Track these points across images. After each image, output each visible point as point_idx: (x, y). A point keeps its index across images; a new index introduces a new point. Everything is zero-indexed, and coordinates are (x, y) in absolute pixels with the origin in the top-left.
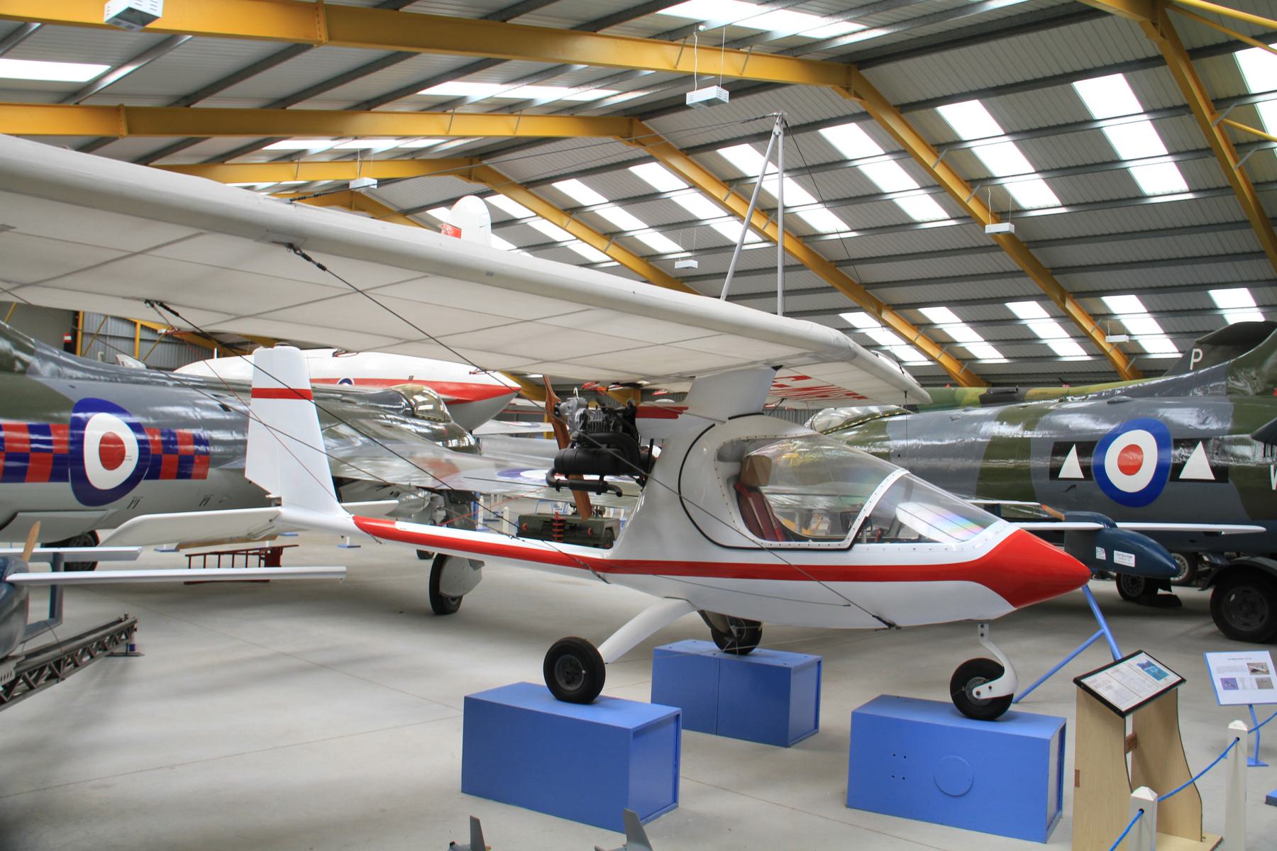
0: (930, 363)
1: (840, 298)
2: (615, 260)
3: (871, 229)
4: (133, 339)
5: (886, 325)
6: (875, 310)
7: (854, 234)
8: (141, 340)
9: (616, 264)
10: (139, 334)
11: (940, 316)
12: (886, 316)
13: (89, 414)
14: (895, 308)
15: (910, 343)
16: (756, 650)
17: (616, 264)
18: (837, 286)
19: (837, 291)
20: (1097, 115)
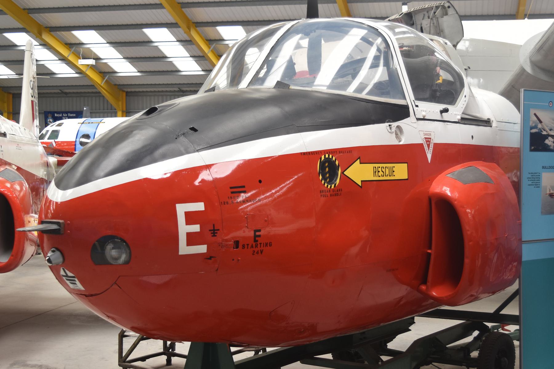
5: (45, 45)
15: (63, 59)
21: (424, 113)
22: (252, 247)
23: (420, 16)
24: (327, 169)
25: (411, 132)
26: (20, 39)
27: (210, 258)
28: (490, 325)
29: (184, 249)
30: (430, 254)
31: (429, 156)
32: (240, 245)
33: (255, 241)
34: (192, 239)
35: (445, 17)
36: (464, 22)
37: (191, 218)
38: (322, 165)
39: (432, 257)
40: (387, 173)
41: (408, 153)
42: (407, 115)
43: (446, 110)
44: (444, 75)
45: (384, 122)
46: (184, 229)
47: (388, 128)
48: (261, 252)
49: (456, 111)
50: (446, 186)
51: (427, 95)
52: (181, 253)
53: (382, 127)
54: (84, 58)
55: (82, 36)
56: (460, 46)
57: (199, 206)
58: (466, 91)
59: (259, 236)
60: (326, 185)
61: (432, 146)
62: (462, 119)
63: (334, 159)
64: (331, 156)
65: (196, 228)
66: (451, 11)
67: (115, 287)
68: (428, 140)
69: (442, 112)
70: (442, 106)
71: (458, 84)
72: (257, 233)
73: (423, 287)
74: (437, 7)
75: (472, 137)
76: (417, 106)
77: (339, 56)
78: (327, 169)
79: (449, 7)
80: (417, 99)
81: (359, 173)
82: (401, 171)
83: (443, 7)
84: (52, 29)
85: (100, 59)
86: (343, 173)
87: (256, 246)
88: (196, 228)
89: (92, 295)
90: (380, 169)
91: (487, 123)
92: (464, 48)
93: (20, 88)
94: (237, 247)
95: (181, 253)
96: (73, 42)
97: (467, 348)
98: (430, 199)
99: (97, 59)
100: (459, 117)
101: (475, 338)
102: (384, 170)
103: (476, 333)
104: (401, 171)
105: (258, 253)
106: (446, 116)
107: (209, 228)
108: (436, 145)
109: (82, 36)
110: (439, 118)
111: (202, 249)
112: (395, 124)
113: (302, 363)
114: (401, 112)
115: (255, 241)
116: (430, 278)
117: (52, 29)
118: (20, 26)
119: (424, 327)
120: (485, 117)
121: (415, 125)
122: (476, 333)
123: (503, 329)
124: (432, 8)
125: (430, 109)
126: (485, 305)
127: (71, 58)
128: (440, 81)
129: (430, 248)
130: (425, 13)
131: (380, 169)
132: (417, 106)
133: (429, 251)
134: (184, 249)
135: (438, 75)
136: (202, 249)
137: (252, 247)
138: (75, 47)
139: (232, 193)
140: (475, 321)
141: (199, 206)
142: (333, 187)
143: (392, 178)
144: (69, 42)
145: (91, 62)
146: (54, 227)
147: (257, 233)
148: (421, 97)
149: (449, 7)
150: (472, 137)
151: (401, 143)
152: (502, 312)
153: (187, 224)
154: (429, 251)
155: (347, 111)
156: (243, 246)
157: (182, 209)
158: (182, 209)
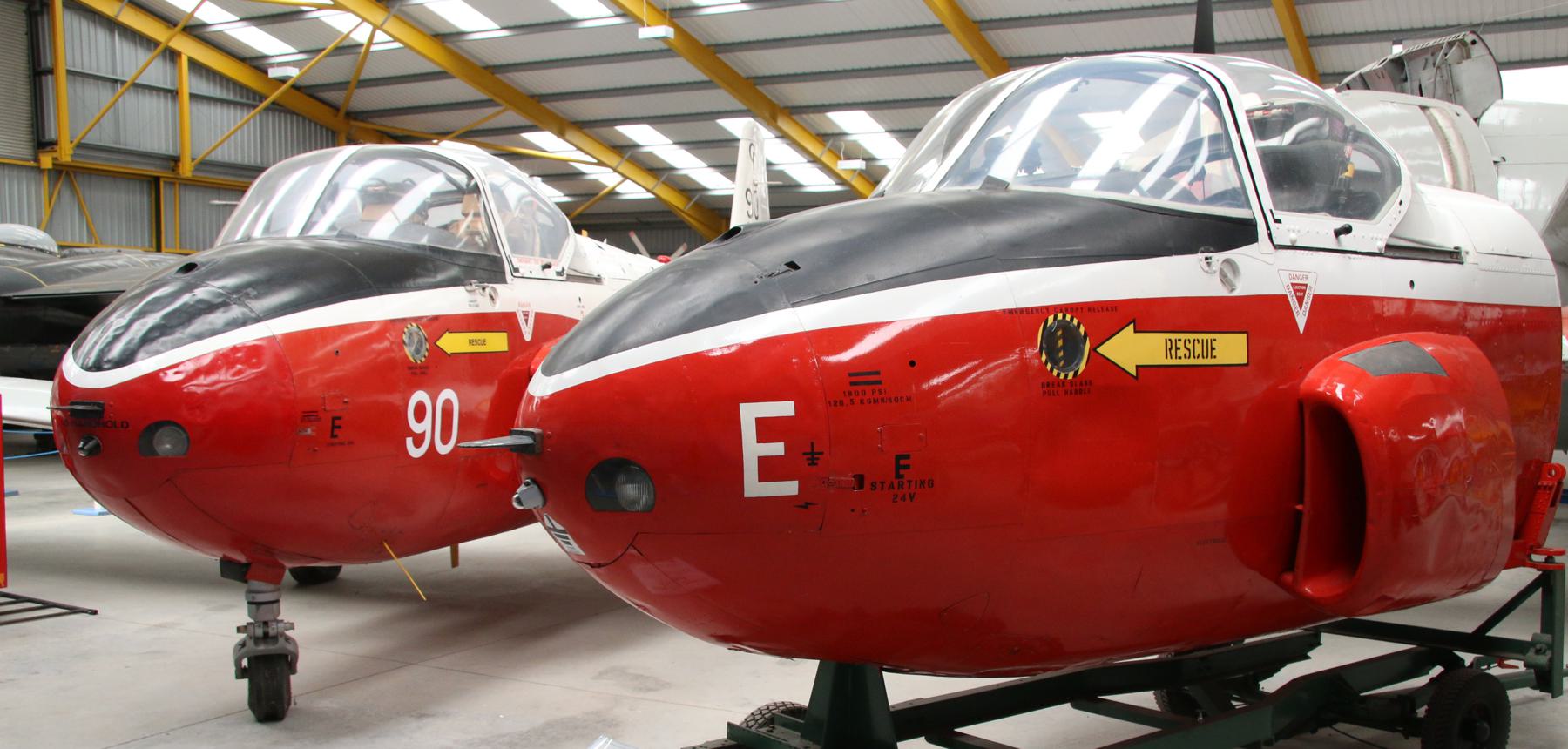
0: (838, 188)
1: (511, 117)
2: (396, 39)
3: (522, 27)
4: (173, 94)
5: (783, 136)
6: (767, 115)
7: (505, 33)
8: (193, 96)
9: (397, 45)
10: (189, 83)
11: (644, 136)
12: (784, 124)
13: (983, 193)
14: (582, 126)
15: (814, 160)
16: (1221, 509)
17: (397, 45)
18: (716, 80)
19: (717, 87)
20: (189, 10)
21: (1293, 236)
22: (891, 486)
23: (1421, 61)
24: (1060, 343)
25: (1257, 271)
26: (736, 126)
27: (806, 506)
28: (1468, 658)
29: (754, 487)
30: (1300, 513)
31: (1301, 320)
32: (867, 484)
33: (899, 476)
34: (769, 470)
35: (1466, 63)
36: (1504, 74)
37: (767, 429)
38: (1049, 336)
39: (1306, 520)
40: (1198, 350)
41: (1259, 316)
42: (1253, 238)
43: (1347, 230)
44: (1359, 161)
45: (1195, 252)
46: (753, 450)
47: (1204, 263)
48: (911, 498)
49: (1370, 233)
50: (1344, 377)
51: (1321, 201)
52: (748, 494)
53: (1193, 261)
54: (848, 158)
55: (842, 120)
56: (1491, 117)
57: (786, 409)
58: (1404, 192)
59: (907, 467)
60: (1055, 372)
61: (1308, 300)
62: (1388, 247)
63: (1075, 321)
64: (1068, 317)
65: (777, 449)
66: (1477, 51)
67: (632, 551)
68: (1300, 290)
69: (1338, 233)
70: (1340, 222)
71: (1388, 178)
72: (902, 462)
73: (1288, 578)
74: (1451, 44)
75: (1412, 283)
76: (1278, 221)
77: (1126, 124)
78: (1060, 343)
79: (1474, 42)
80: (1277, 205)
81: (1131, 350)
82: (1231, 349)
83: (1463, 43)
84: (794, 111)
85: (874, 159)
86: (1093, 350)
87: (901, 486)
88: (777, 449)
89: (599, 566)
90: (1180, 344)
91: (1453, 256)
92: (1495, 122)
93: (729, 210)
94: (861, 486)
95: (748, 494)
96: (829, 131)
97: (1410, 698)
98: (1301, 405)
99: (869, 159)
100: (1382, 244)
101: (1432, 680)
102: (1190, 346)
103: (1437, 671)
104: (1231, 349)
105: (903, 498)
106: (1346, 242)
107: (802, 448)
108: (1318, 299)
109: (842, 120)
110: (1332, 245)
111: (790, 488)
112: (1218, 257)
113: (1075, 706)
114: (1240, 233)
115: (899, 476)
116: (1301, 559)
117: (794, 111)
118: (743, 107)
119: (1336, 652)
120: (1450, 246)
121: (1269, 259)
122: (1437, 671)
123: (1501, 665)
124: (1440, 46)
125: (1318, 226)
126: (1453, 614)
127: (826, 159)
128: (1349, 174)
129: (1301, 501)
130: (1429, 56)
131: (1180, 344)
132: (1278, 221)
133: (1299, 507)
134: (754, 487)
135: (1345, 162)
136: (790, 488)
137: (891, 486)
138: (832, 140)
139: (853, 384)
140: (1434, 646)
141: (786, 409)
142: (1070, 376)
143: (1209, 361)
144: (823, 131)
145: (859, 164)
146: (527, 440)
147: (902, 462)
148: (1308, 205)
149: (1474, 42)
150: (1412, 283)
151: (1236, 293)
152: (1491, 633)
153: (760, 440)
154: (1299, 507)
155: (1144, 229)
156: (873, 485)
157: (750, 413)
158: (750, 413)
